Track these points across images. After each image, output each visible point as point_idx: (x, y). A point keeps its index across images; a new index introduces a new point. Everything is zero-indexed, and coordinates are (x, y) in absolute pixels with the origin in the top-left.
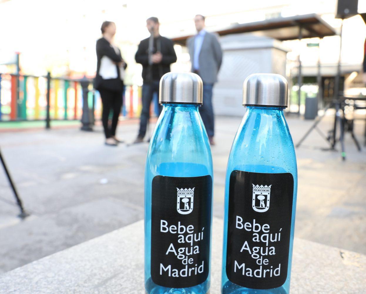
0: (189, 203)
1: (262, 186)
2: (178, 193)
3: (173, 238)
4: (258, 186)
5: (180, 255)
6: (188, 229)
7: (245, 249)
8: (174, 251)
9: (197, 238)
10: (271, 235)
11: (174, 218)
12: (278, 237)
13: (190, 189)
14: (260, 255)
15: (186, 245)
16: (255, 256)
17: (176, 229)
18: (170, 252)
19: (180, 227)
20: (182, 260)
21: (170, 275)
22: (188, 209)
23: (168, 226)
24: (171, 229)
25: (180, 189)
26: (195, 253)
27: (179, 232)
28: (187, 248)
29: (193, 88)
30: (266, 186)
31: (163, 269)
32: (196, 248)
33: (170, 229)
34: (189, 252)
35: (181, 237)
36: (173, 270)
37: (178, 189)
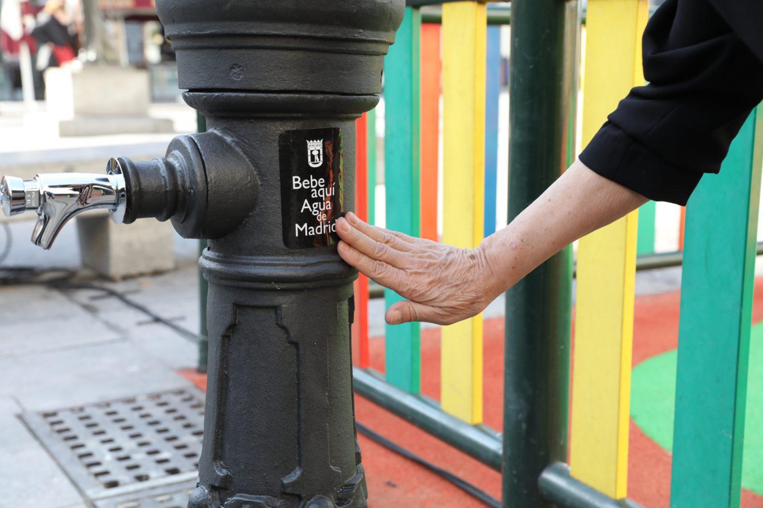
0: (319, 155)
1: (315, 141)
2: (308, 145)
3: (305, 194)
4: (311, 141)
5: (315, 211)
6: (319, 182)
7: (306, 207)
8: (309, 207)
9: (328, 193)
10: (326, 189)
11: (306, 172)
12: (332, 192)
13: (318, 141)
14: (319, 211)
15: (319, 199)
16: (315, 213)
17: (309, 183)
18: (305, 209)
19: (312, 180)
20: (317, 216)
21: (306, 235)
22: (318, 161)
23: (301, 182)
24: (304, 184)
25: (309, 141)
26: (327, 209)
27: (312, 187)
28: (320, 203)
29: (207, 51)
30: (318, 141)
31: (298, 229)
32: (328, 204)
33: (304, 184)
34: (322, 207)
35: (314, 192)
36: (310, 228)
37: (308, 142)
